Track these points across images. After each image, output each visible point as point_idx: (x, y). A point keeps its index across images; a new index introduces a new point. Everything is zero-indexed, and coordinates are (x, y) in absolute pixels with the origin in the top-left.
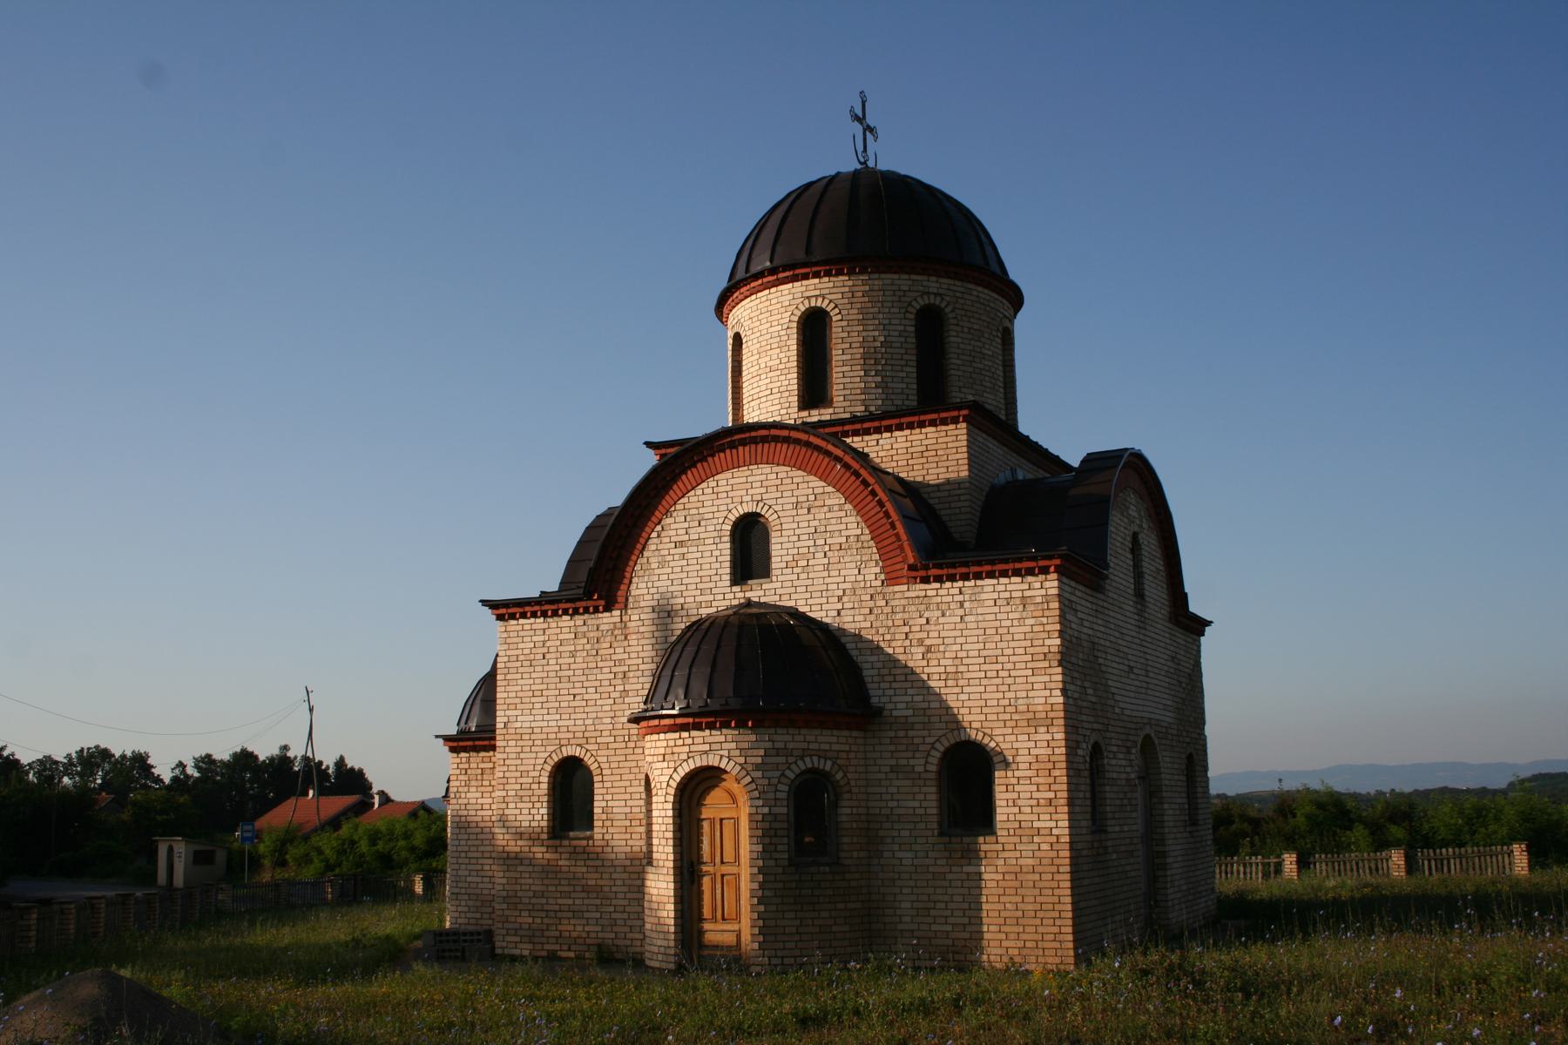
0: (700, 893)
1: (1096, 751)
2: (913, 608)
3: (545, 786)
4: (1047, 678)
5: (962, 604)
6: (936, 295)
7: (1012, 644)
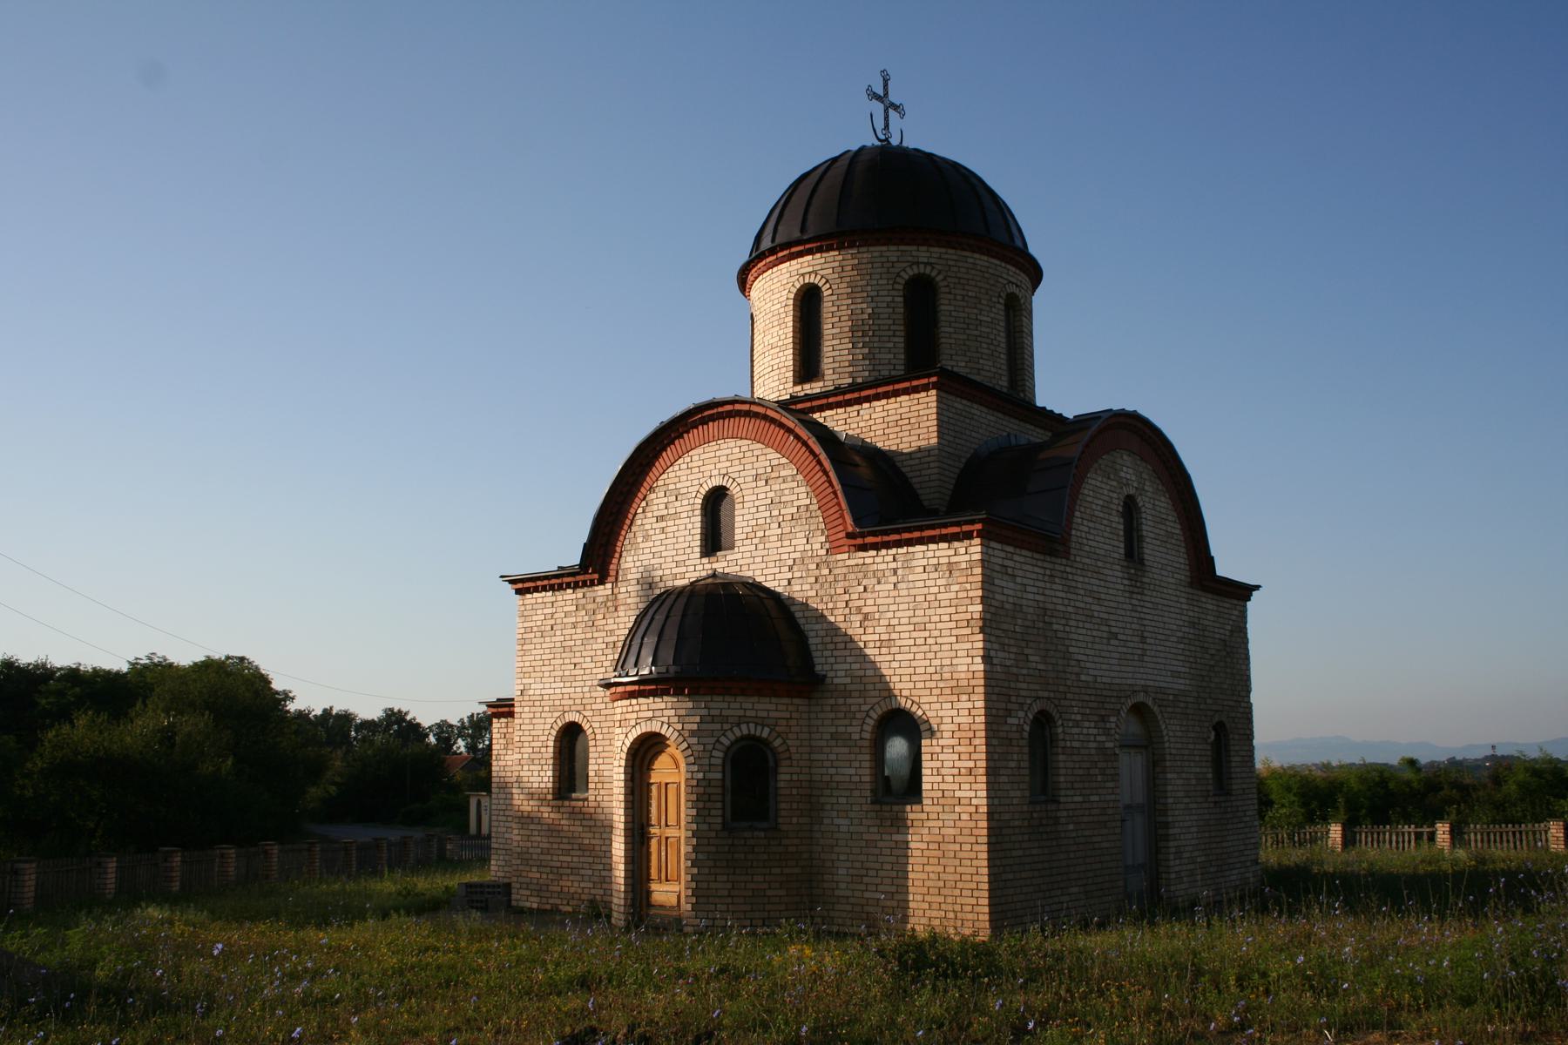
0: (649, 854)
1: (1043, 722)
2: (852, 576)
3: (551, 750)
4: (969, 645)
5: (895, 571)
6: (926, 264)
7: (939, 611)
